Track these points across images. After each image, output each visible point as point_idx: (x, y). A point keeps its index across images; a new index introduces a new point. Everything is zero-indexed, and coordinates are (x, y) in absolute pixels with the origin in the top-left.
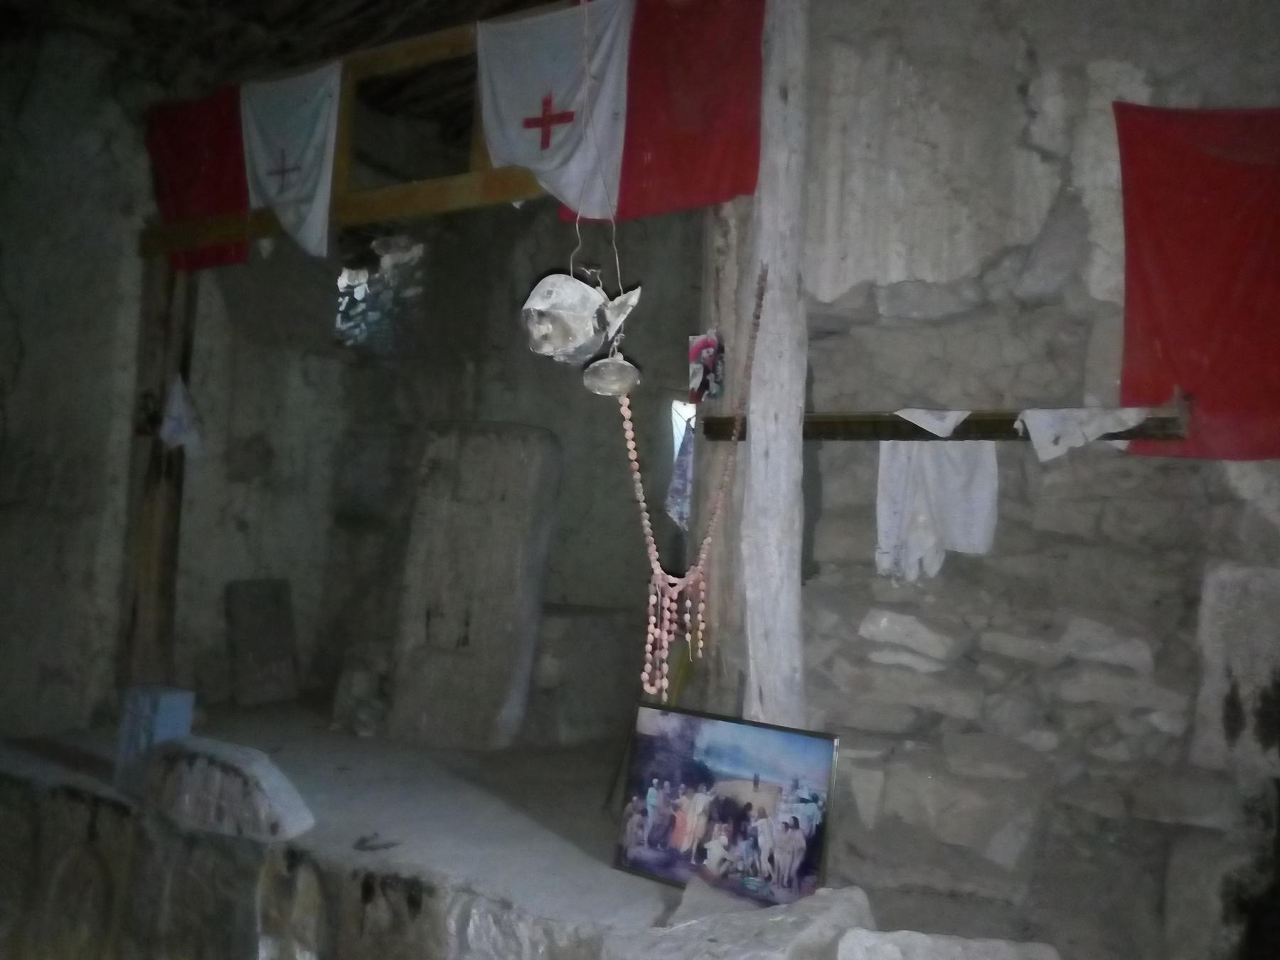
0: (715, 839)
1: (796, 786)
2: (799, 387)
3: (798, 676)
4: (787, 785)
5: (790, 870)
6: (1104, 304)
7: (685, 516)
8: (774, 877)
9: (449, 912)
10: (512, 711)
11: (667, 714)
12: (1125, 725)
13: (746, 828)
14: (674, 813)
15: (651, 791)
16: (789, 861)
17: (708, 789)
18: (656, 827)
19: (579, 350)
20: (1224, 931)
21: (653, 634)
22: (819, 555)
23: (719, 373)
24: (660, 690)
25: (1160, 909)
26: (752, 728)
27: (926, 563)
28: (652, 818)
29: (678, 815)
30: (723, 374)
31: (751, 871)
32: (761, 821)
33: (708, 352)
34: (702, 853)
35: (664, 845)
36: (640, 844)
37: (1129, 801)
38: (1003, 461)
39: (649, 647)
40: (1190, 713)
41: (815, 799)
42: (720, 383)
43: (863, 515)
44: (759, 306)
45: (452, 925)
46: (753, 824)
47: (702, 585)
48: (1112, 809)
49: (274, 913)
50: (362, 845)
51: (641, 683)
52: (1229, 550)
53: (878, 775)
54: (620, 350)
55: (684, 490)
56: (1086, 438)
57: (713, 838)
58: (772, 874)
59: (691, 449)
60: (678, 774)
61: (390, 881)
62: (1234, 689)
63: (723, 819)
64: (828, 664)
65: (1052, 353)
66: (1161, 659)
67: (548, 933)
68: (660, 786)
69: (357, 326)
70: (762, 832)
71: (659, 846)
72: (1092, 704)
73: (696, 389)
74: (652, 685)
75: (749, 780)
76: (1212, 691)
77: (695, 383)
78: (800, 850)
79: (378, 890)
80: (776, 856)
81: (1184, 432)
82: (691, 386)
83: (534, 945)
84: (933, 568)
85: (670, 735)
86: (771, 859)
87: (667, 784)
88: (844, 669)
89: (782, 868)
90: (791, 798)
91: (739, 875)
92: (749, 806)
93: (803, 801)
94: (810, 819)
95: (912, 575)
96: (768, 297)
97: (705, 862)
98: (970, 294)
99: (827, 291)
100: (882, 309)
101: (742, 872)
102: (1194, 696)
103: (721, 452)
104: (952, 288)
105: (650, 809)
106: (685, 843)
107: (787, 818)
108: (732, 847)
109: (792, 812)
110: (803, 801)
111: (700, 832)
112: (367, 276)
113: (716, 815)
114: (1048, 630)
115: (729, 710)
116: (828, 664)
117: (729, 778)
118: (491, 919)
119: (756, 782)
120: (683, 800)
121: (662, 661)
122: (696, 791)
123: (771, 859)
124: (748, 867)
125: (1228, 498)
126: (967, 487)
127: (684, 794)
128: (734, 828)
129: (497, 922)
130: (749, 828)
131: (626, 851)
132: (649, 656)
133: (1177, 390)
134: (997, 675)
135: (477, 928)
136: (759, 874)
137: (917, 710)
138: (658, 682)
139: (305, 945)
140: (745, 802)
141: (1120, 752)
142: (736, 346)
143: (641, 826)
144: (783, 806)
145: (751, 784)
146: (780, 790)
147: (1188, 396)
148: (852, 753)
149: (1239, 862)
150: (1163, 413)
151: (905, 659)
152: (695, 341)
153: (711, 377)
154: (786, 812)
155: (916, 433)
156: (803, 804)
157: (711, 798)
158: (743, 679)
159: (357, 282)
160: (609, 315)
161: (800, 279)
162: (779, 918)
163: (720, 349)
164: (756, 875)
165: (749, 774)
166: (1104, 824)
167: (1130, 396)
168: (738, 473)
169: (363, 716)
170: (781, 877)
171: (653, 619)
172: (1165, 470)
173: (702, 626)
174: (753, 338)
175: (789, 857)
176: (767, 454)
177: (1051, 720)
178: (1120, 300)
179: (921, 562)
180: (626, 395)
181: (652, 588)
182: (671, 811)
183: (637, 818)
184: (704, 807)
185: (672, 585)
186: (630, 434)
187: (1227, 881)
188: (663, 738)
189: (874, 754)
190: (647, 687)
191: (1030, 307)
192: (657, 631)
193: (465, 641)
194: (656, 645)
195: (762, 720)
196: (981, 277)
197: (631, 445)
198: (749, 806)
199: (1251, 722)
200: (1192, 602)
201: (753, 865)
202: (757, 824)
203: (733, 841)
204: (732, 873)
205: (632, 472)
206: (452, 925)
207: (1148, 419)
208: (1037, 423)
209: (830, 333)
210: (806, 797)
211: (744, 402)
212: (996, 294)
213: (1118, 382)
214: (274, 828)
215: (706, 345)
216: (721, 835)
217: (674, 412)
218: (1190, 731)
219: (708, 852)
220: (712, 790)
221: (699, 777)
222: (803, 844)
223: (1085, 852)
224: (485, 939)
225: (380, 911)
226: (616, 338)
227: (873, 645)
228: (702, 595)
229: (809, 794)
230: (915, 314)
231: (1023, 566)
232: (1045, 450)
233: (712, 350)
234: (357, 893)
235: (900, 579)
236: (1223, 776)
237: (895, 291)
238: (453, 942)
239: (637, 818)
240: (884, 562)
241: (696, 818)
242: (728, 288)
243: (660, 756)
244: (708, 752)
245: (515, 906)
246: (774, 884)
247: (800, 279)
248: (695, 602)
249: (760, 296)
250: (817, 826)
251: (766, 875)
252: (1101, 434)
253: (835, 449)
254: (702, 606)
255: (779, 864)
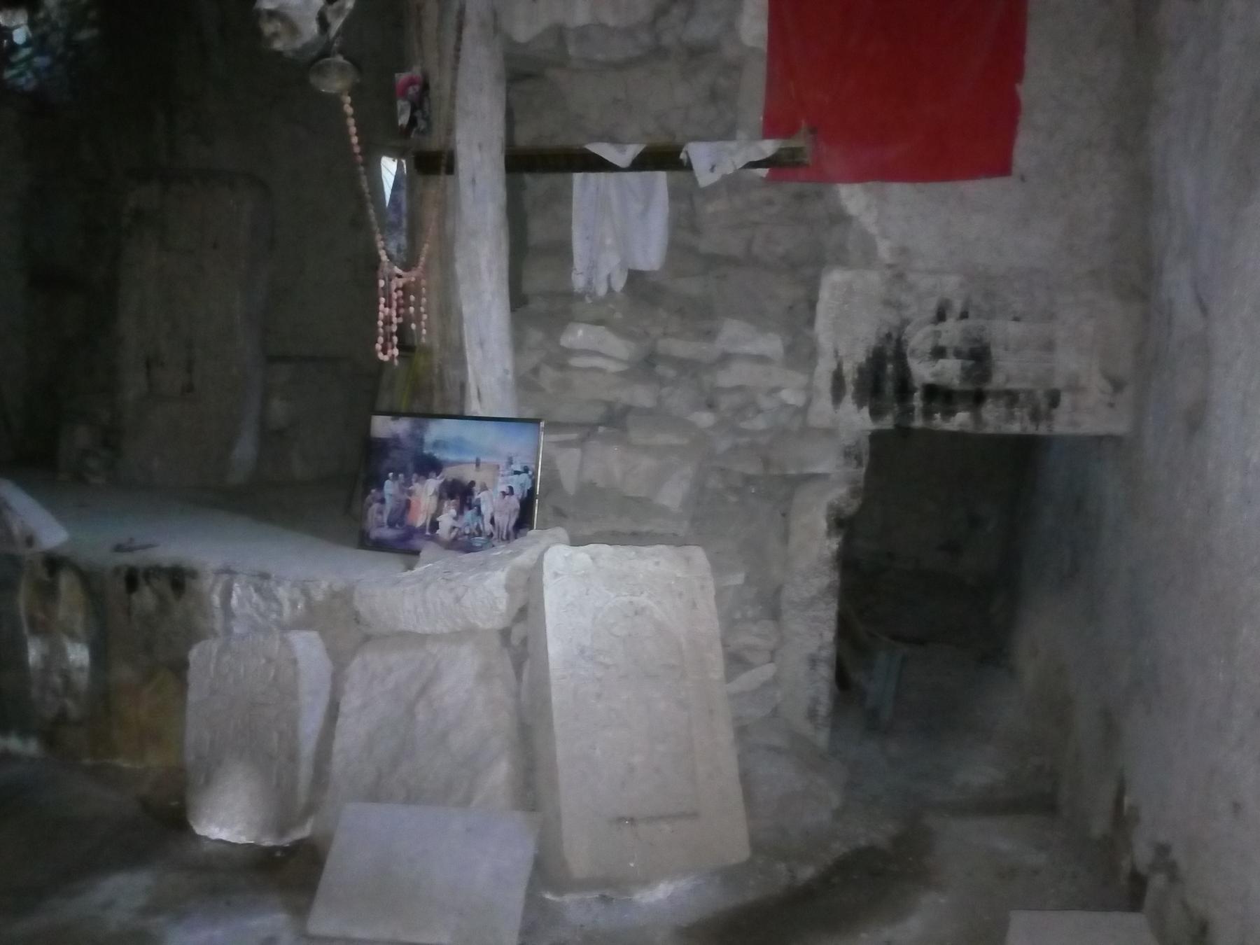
0: (446, 513)
1: (510, 462)
2: (499, 119)
3: (510, 377)
4: (503, 462)
5: (508, 526)
6: (753, 50)
7: (403, 248)
8: (495, 534)
9: (212, 589)
10: (245, 450)
11: (398, 419)
12: (765, 403)
13: (470, 500)
14: (409, 498)
15: (388, 483)
16: (506, 520)
17: (437, 475)
18: (393, 512)
19: (306, 47)
20: (827, 543)
21: (383, 312)
22: (528, 287)
23: (426, 109)
24: (392, 357)
25: (785, 537)
26: (470, 421)
27: (613, 280)
28: (389, 504)
29: (413, 499)
30: (430, 111)
31: (477, 533)
32: (483, 493)
33: (415, 90)
34: (435, 525)
35: (401, 524)
36: (380, 526)
37: (767, 462)
38: (675, 194)
39: (380, 323)
40: (809, 390)
41: (526, 470)
42: (427, 120)
43: (561, 251)
44: (459, 39)
45: (216, 600)
46: (476, 497)
47: (423, 282)
48: (753, 469)
49: (40, 615)
50: (119, 548)
51: (375, 353)
52: (841, 260)
53: (576, 452)
54: (341, 52)
55: (400, 223)
56: (735, 166)
57: (444, 512)
58: (494, 533)
59: (404, 185)
60: (411, 466)
61: (153, 572)
62: (840, 366)
63: (451, 496)
64: (535, 371)
65: (714, 96)
66: (790, 349)
67: (306, 593)
68: (396, 477)
69: (21, 75)
70: (484, 501)
71: (397, 526)
72: (739, 389)
73: (405, 127)
74: (385, 352)
75: (471, 463)
76: (825, 368)
77: (403, 120)
78: (515, 510)
79: (142, 581)
80: (496, 518)
81: (807, 160)
82: (400, 123)
83: (294, 604)
84: (619, 283)
85: (401, 436)
86: (492, 521)
87: (401, 476)
88: (549, 375)
89: (501, 527)
90: (506, 472)
91: (466, 537)
92: (473, 483)
93: (517, 473)
94: (522, 486)
95: (602, 290)
96: (468, 32)
97: (438, 532)
98: (645, 38)
99: (523, 32)
100: (572, 50)
101: (469, 535)
102: (811, 374)
103: (433, 188)
104: (629, 32)
105: (387, 498)
106: (420, 519)
107: (505, 488)
108: (460, 516)
109: (508, 483)
110: (517, 473)
111: (432, 509)
112: (26, 17)
113: (445, 494)
114: (710, 335)
115: (455, 412)
116: (535, 371)
117: (453, 464)
118: (252, 589)
119: (478, 463)
120: (416, 487)
121: (392, 334)
122: (427, 478)
123: (492, 521)
124: (474, 531)
125: (840, 218)
126: (644, 213)
127: (417, 481)
128: (461, 503)
129: (258, 590)
130: (474, 501)
131: (368, 534)
132: (381, 330)
133: (804, 125)
134: (671, 373)
135: (240, 599)
136: (483, 534)
137: (609, 405)
138: (389, 351)
139: (73, 636)
140: (469, 482)
141: (759, 423)
142: (440, 82)
143: (380, 512)
144: (500, 480)
145: (474, 465)
146: (498, 467)
147: (813, 130)
148: (554, 437)
149: (838, 493)
150: (794, 143)
151: (598, 362)
152: (402, 78)
153: (418, 114)
154: (503, 483)
155: (601, 165)
156: (517, 476)
157: (442, 481)
158: (463, 387)
159: (14, 24)
160: (330, 17)
161: (495, 15)
162: (499, 553)
163: (425, 87)
164: (480, 535)
165: (473, 459)
166: (748, 480)
167: (771, 128)
168: (447, 208)
169: (93, 463)
170: (500, 533)
171: (383, 300)
172: (800, 197)
173: (425, 317)
174: (455, 69)
175: (507, 518)
176: (473, 181)
177: (711, 406)
178: (763, 46)
179: (609, 278)
180: (347, 92)
181: (380, 274)
182: (406, 496)
183: (376, 506)
184: (435, 489)
185: (400, 276)
186: (353, 130)
187: (831, 507)
188: (396, 439)
189: (574, 436)
190: (381, 356)
191: (697, 54)
192: (387, 310)
193: (189, 388)
194: (388, 321)
195: (481, 414)
196: (654, 22)
197: (355, 140)
198: (473, 483)
199: (850, 388)
200: (812, 304)
201: (478, 528)
202: (480, 496)
203: (460, 512)
204: (461, 537)
205: (359, 143)
206: (216, 600)
207: (781, 150)
208: (699, 154)
209: (528, 76)
210: (519, 469)
211: (450, 130)
212: (668, 39)
213: (761, 118)
214: (30, 541)
215: (412, 82)
216: (450, 509)
217: (382, 167)
218: (809, 402)
219: (440, 524)
220: (441, 475)
221: (429, 466)
222: (518, 506)
223: (733, 499)
224: (248, 606)
225: (146, 598)
226: (336, 40)
227: (570, 352)
228: (424, 290)
229: (521, 467)
230: (600, 57)
231: (692, 287)
232: (705, 178)
233: (417, 88)
234: (121, 586)
235: (593, 295)
236: (830, 433)
237: (583, 34)
238: (218, 614)
239: (376, 506)
240: (579, 282)
241: (428, 499)
242: (430, 25)
243: (395, 454)
244: (436, 444)
245: (273, 575)
246: (495, 539)
247: (495, 15)
248: (419, 296)
249: (460, 28)
250: (528, 490)
251: (489, 534)
252: (745, 163)
253: (537, 184)
254: (424, 300)
255: (498, 523)
